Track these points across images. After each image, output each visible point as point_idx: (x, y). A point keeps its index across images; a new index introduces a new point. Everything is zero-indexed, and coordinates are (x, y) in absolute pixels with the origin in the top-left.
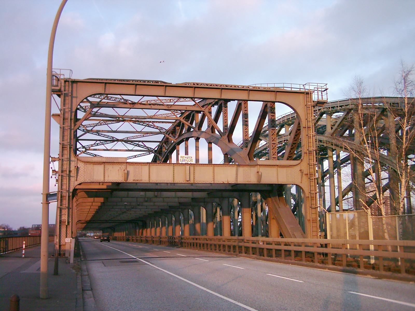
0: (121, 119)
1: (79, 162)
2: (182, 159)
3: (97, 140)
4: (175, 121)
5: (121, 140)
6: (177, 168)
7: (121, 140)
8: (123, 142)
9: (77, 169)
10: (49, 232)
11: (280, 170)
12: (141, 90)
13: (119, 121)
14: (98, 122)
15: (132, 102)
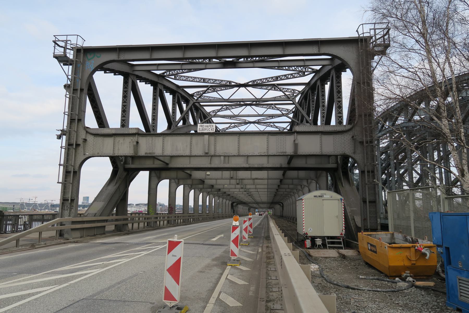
0: (242, 103)
1: (88, 135)
2: (201, 128)
3: (231, 123)
4: (147, 81)
5: (254, 123)
6: (195, 139)
7: (254, 123)
8: (256, 124)
9: (85, 140)
10: (317, 190)
11: (325, 137)
12: (156, 55)
13: (242, 105)
14: (220, 107)
15: (236, 83)
